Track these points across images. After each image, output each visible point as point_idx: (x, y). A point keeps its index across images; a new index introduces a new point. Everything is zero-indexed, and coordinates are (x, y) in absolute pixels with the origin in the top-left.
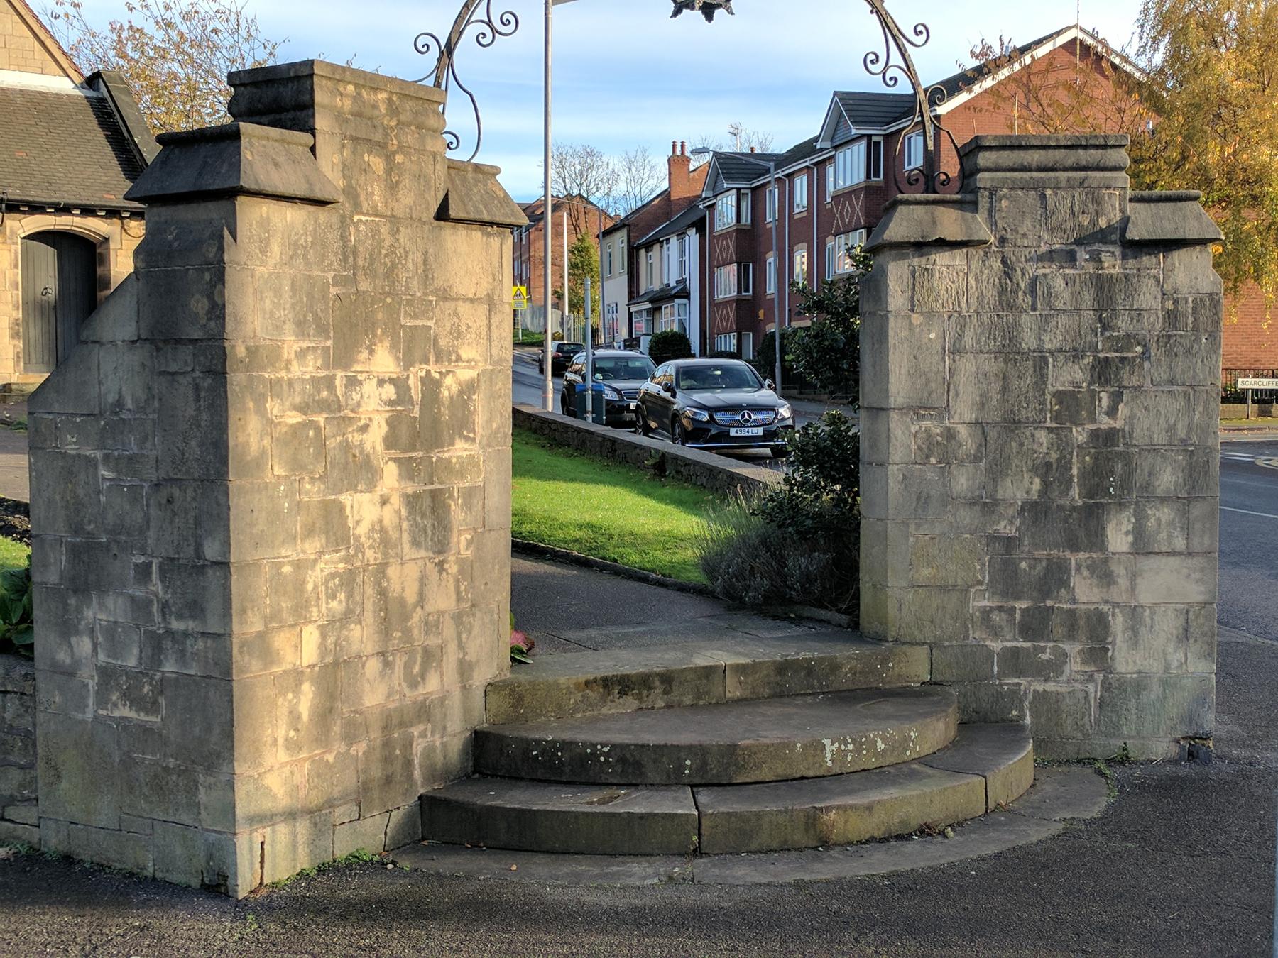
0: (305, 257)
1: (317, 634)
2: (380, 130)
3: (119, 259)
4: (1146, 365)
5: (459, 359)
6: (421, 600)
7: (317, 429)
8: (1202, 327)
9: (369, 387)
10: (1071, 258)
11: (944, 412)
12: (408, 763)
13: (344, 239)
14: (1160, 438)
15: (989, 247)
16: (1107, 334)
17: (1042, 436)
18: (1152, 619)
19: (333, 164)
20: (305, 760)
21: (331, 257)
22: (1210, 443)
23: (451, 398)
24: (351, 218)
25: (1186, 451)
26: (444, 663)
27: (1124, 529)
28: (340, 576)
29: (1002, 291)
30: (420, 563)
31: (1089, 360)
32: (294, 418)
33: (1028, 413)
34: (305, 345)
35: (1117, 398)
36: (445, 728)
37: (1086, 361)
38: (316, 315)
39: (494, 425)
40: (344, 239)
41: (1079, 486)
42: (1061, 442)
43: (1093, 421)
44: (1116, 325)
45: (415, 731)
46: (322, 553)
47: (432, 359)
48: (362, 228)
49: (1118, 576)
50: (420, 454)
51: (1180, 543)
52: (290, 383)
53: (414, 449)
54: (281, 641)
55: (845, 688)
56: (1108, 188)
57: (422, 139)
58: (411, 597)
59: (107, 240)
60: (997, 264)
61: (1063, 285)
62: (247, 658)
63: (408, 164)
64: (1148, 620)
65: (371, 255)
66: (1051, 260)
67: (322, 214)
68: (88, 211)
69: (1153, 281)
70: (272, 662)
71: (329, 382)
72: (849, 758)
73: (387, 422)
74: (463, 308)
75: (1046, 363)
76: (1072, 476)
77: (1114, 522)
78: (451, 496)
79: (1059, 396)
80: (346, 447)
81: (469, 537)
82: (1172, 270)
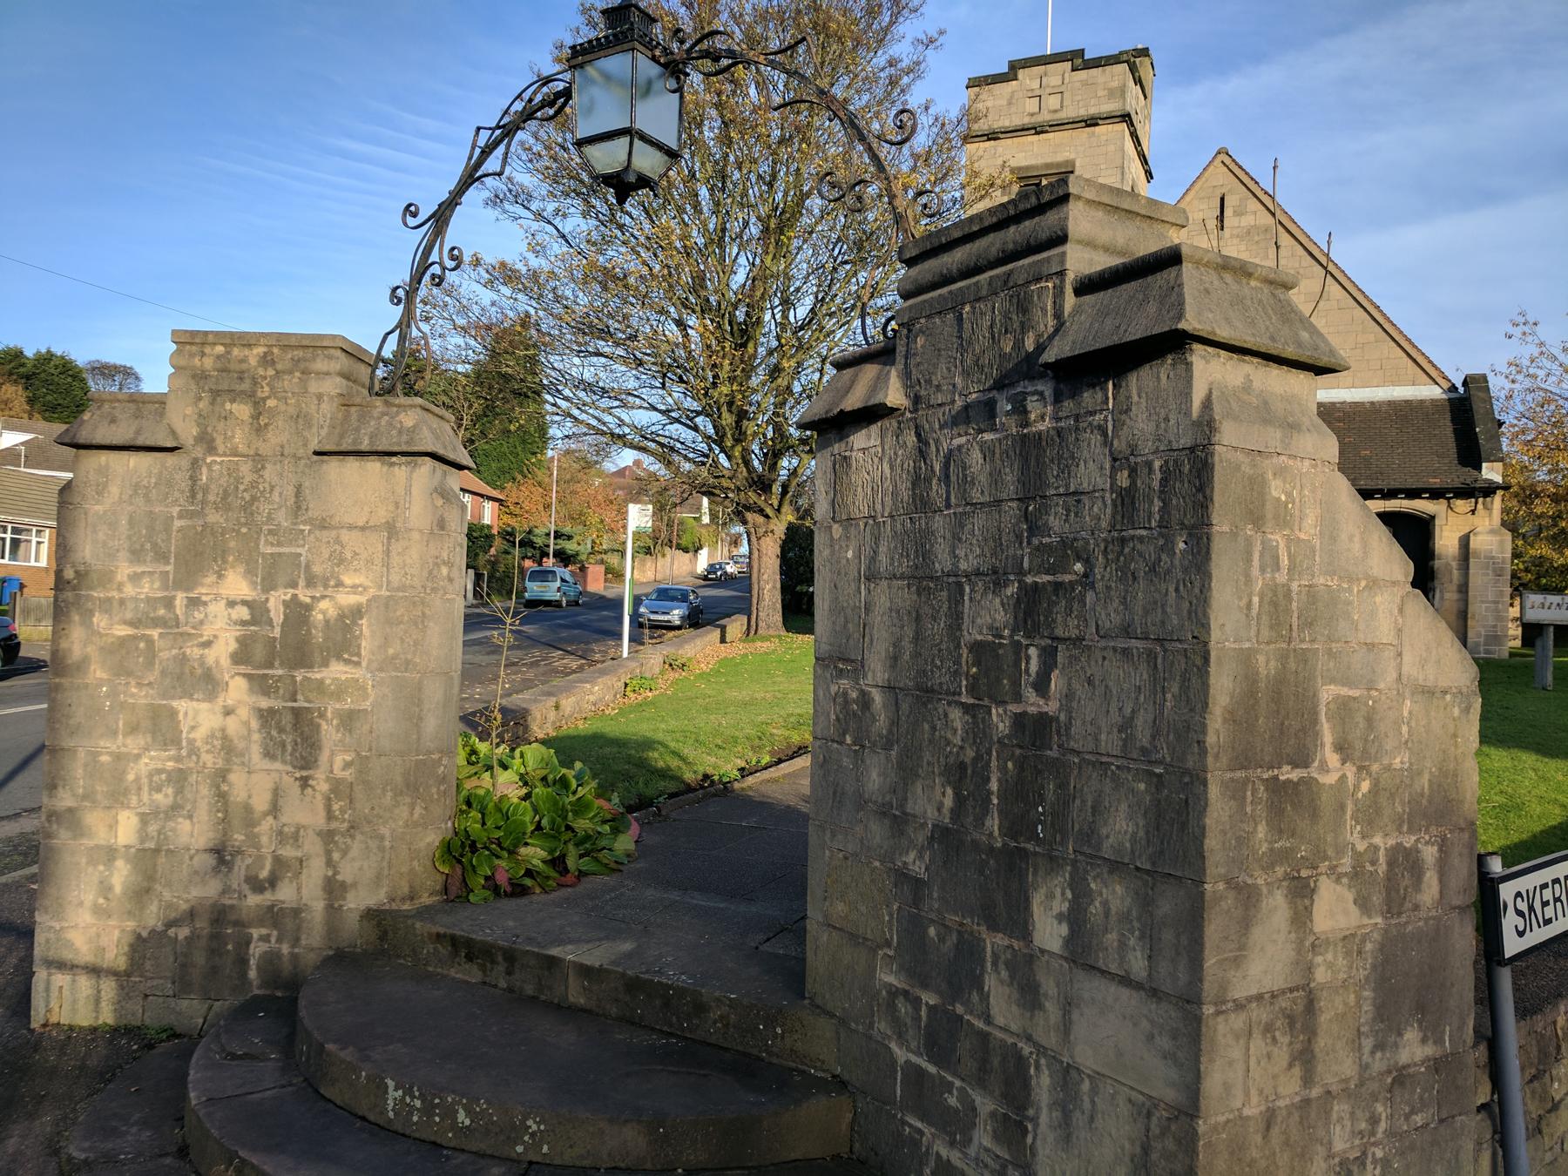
0: (146, 496)
1: (135, 820)
2: (248, 381)
3: (1445, 534)
4: (1090, 597)
5: (340, 584)
6: (275, 809)
7: (150, 641)
8: (1175, 516)
9: (217, 609)
10: (989, 408)
11: (857, 668)
12: (243, 962)
13: (194, 479)
14: (1110, 742)
15: (903, 415)
16: (1035, 541)
17: (956, 715)
18: (1093, 1102)
19: (185, 416)
20: (114, 927)
21: (177, 494)
22: (1190, 764)
23: (327, 622)
24: (204, 460)
25: (1151, 774)
26: (303, 877)
27: (1056, 910)
28: (169, 773)
29: (916, 482)
30: (275, 775)
31: (1012, 590)
32: (122, 631)
33: (940, 678)
34: (139, 570)
35: (1049, 659)
36: (297, 940)
37: (1009, 591)
38: (155, 545)
39: (391, 651)
40: (194, 479)
41: (1000, 812)
42: (978, 730)
43: (1018, 697)
44: (1046, 524)
45: (255, 933)
46: (147, 749)
47: (302, 583)
48: (216, 467)
49: (1046, 995)
50: (280, 672)
51: (1138, 965)
52: (122, 602)
53: (271, 666)
54: (94, 819)
55: (713, 1040)
56: (1038, 280)
57: (303, 383)
58: (261, 803)
59: (1433, 518)
60: (911, 439)
61: (981, 461)
62: (55, 827)
63: (283, 407)
64: (1087, 1105)
65: (225, 491)
66: (967, 421)
67: (170, 459)
68: (1413, 494)
69: (1096, 438)
70: (82, 835)
71: (169, 603)
72: (415, 1119)
73: (237, 640)
74: (345, 536)
75: (962, 594)
76: (990, 793)
77: (1043, 891)
78: (322, 715)
79: (977, 647)
80: (183, 659)
81: (348, 758)
82: (1128, 410)
